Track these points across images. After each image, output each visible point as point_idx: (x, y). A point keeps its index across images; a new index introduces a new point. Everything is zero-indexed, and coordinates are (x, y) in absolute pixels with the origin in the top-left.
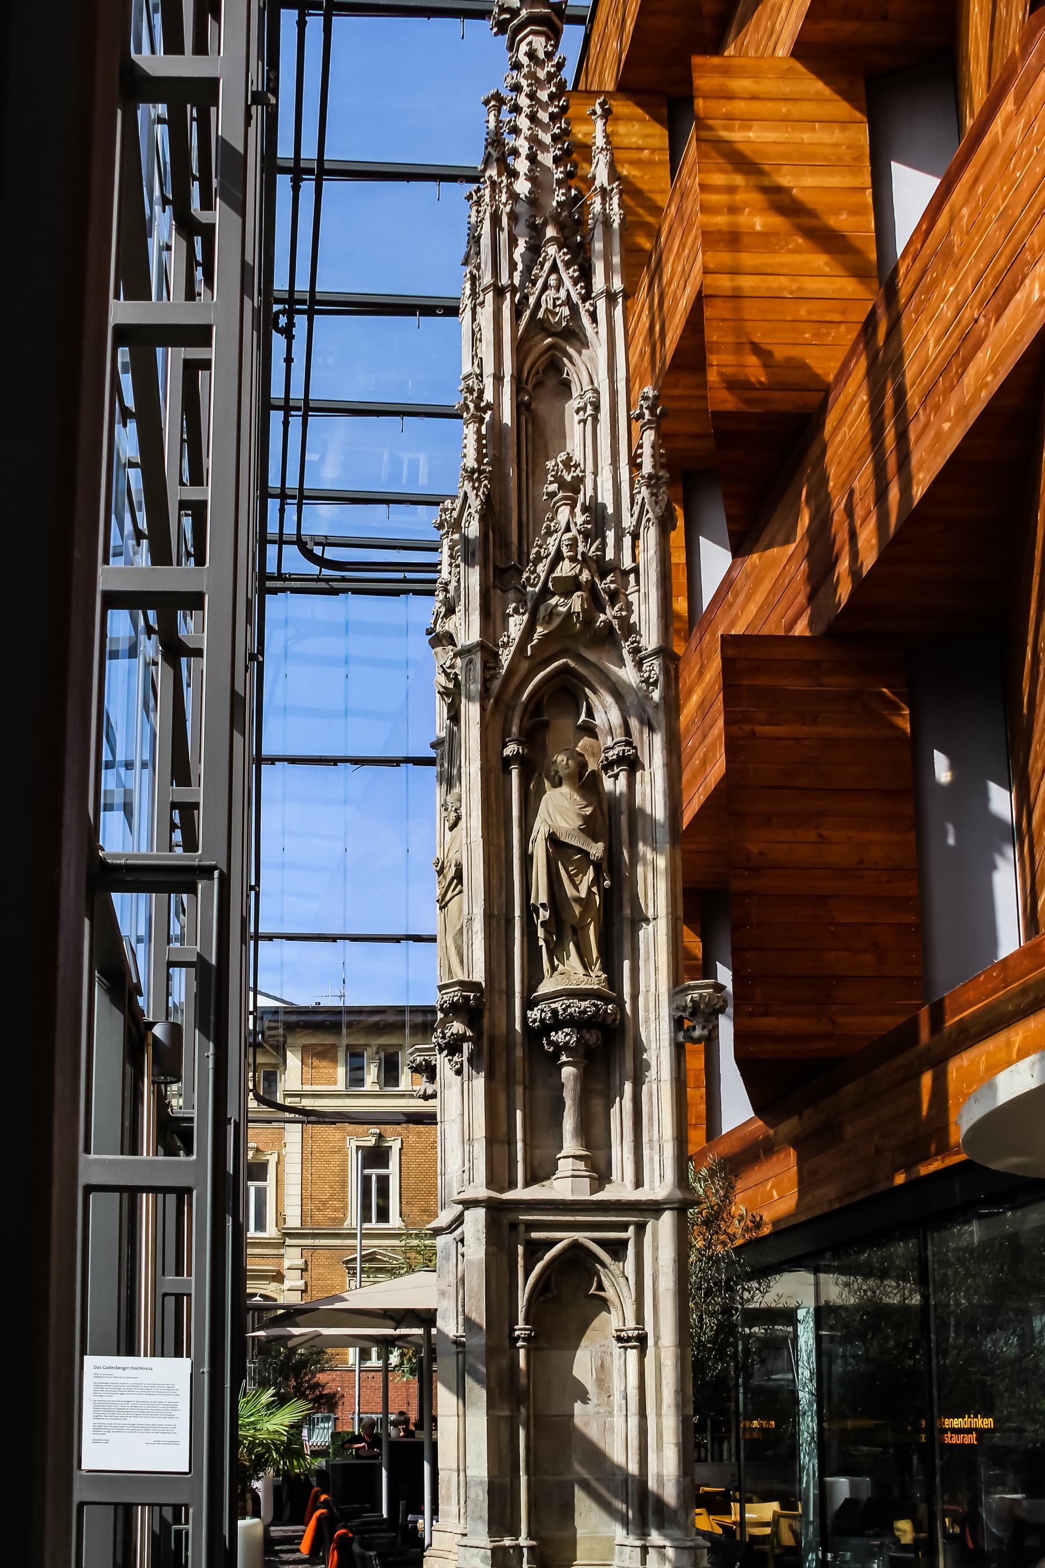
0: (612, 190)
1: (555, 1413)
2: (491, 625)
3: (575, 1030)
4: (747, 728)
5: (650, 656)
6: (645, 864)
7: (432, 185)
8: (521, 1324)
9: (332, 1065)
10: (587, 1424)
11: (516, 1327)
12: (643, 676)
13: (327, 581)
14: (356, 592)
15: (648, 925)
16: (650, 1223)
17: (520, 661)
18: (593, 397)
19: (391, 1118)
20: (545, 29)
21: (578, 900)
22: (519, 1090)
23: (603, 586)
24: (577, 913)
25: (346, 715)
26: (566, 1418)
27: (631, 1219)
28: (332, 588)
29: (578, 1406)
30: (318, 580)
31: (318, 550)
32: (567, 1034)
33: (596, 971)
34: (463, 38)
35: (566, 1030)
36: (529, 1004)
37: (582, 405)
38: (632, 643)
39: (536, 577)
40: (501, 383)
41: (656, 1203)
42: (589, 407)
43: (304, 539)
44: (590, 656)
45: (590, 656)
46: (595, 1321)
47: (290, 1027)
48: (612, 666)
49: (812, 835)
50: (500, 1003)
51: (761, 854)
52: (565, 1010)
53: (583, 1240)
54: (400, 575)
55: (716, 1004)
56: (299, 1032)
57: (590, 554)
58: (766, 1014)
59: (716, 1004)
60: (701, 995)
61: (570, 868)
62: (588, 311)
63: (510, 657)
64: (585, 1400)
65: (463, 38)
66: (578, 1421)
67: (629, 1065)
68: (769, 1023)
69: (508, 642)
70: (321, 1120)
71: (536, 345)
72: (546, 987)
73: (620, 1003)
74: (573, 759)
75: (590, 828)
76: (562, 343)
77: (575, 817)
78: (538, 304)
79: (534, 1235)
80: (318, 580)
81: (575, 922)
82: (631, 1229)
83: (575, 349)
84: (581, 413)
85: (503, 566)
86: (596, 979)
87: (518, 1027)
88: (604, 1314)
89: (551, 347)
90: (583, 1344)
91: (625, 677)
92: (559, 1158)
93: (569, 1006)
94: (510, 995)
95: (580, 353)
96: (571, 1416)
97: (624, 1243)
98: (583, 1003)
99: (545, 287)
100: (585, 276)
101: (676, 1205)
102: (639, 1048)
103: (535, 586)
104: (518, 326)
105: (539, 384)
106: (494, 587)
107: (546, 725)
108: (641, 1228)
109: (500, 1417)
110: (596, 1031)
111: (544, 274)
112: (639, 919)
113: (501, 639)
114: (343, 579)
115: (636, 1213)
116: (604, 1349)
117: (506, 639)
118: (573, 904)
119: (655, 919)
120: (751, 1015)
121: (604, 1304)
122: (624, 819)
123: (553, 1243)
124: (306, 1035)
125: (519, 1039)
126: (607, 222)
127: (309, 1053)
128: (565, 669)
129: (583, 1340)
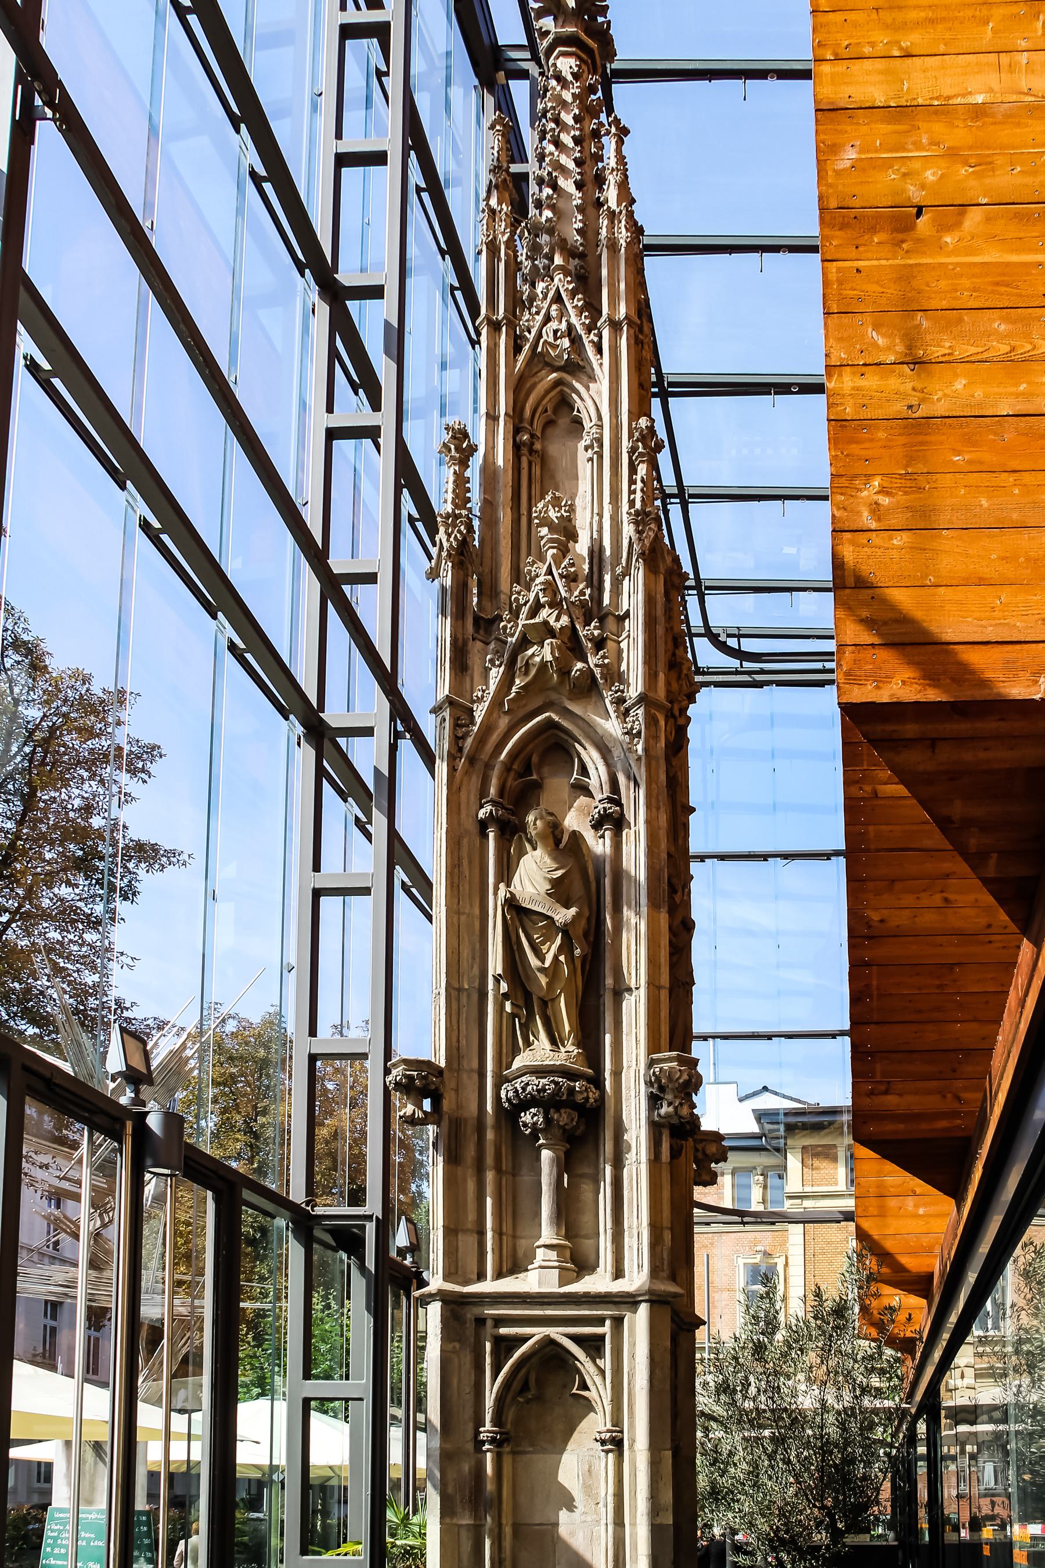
0: (621, 212)
1: (538, 1522)
2: (468, 679)
3: (541, 1110)
4: (868, 788)
5: (634, 705)
6: (628, 931)
7: (756, 256)
8: (488, 1426)
9: (832, 1165)
10: (572, 1534)
11: (482, 1429)
12: (626, 728)
13: (749, 673)
14: (780, 684)
15: (631, 995)
16: (626, 1317)
17: (500, 717)
18: (597, 433)
19: (828, 1216)
20: (574, 49)
21: (542, 970)
22: (490, 1176)
23: (585, 632)
24: (544, 984)
25: (775, 810)
26: (550, 1527)
27: (605, 1312)
28: (755, 681)
29: (563, 1515)
30: (737, 672)
31: (732, 643)
32: (535, 1115)
33: (570, 1047)
34: (745, 99)
35: (532, 1110)
36: (500, 1081)
37: (588, 442)
38: (616, 692)
39: (512, 626)
40: (496, 422)
41: (629, 1295)
42: (595, 445)
43: (714, 630)
44: (575, 708)
45: (575, 708)
46: (582, 1423)
47: (790, 1128)
48: (598, 719)
49: (937, 899)
50: (470, 1084)
51: (882, 921)
52: (524, 1089)
53: (554, 1336)
54: (819, 666)
55: (679, 1078)
56: (798, 1133)
57: (573, 599)
58: (886, 1092)
59: (679, 1078)
60: (661, 1069)
61: (535, 936)
62: (592, 341)
63: (483, 712)
64: (571, 1507)
65: (745, 99)
66: (563, 1531)
67: (609, 1147)
68: (891, 1101)
69: (483, 697)
70: (759, 1220)
71: (540, 381)
72: (518, 1063)
73: (597, 1081)
74: (542, 818)
75: (559, 891)
76: (568, 378)
77: (541, 881)
78: (539, 335)
79: (503, 1331)
80: (737, 672)
81: (542, 994)
82: (608, 1323)
83: (581, 383)
84: (590, 451)
85: (489, 617)
86: (568, 1054)
87: (489, 1108)
88: (592, 1414)
89: (558, 383)
90: (570, 1447)
91: (612, 731)
92: (539, 1247)
93: (527, 1084)
94: (482, 1075)
95: (588, 388)
96: (556, 1525)
97: (602, 1338)
98: (542, 1080)
99: (548, 319)
100: (592, 308)
101: (647, 1297)
102: (619, 1129)
103: (512, 635)
104: (515, 361)
105: (549, 423)
106: (474, 639)
107: (537, 786)
108: (618, 1321)
109: (460, 1526)
110: (568, 1110)
111: (546, 305)
112: (620, 991)
113: (475, 694)
114: (762, 672)
115: (611, 1306)
116: (591, 1453)
117: (480, 694)
118: (538, 974)
119: (637, 988)
120: (871, 1093)
121: (588, 1407)
122: (608, 881)
123: (525, 1339)
124: (804, 1136)
125: (490, 1120)
126: (613, 246)
127: (809, 1153)
128: (550, 725)
129: (569, 1443)
